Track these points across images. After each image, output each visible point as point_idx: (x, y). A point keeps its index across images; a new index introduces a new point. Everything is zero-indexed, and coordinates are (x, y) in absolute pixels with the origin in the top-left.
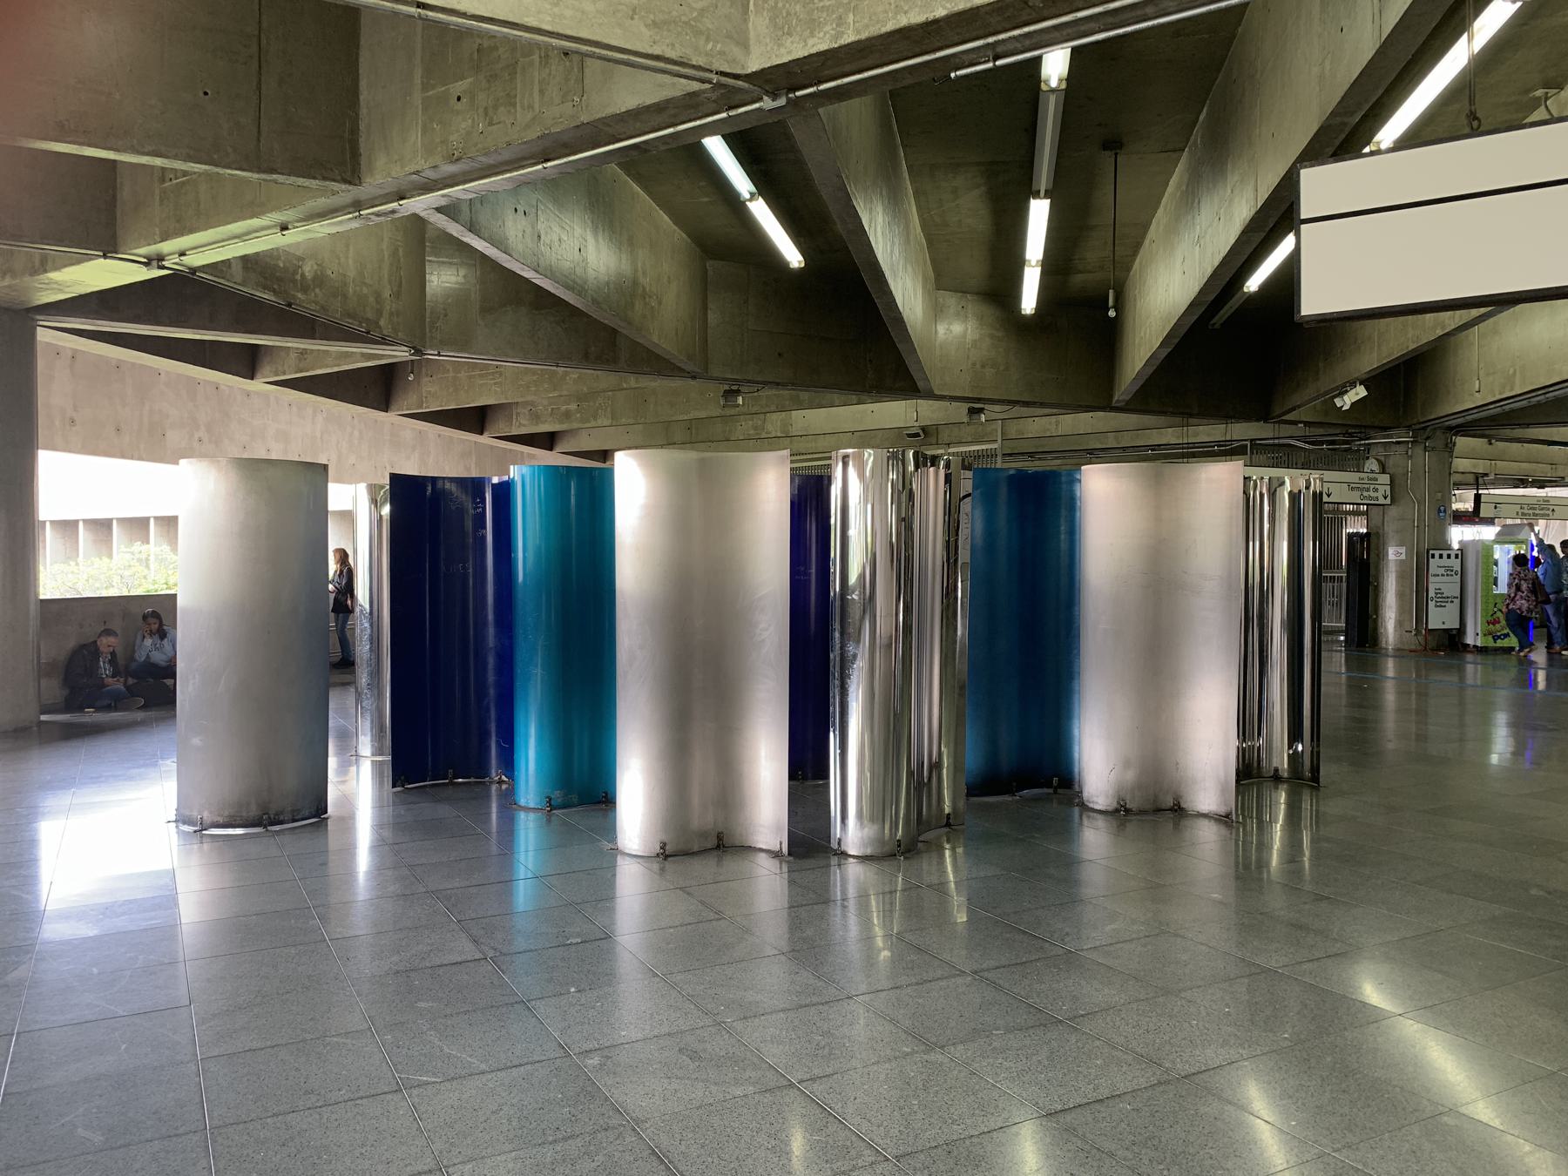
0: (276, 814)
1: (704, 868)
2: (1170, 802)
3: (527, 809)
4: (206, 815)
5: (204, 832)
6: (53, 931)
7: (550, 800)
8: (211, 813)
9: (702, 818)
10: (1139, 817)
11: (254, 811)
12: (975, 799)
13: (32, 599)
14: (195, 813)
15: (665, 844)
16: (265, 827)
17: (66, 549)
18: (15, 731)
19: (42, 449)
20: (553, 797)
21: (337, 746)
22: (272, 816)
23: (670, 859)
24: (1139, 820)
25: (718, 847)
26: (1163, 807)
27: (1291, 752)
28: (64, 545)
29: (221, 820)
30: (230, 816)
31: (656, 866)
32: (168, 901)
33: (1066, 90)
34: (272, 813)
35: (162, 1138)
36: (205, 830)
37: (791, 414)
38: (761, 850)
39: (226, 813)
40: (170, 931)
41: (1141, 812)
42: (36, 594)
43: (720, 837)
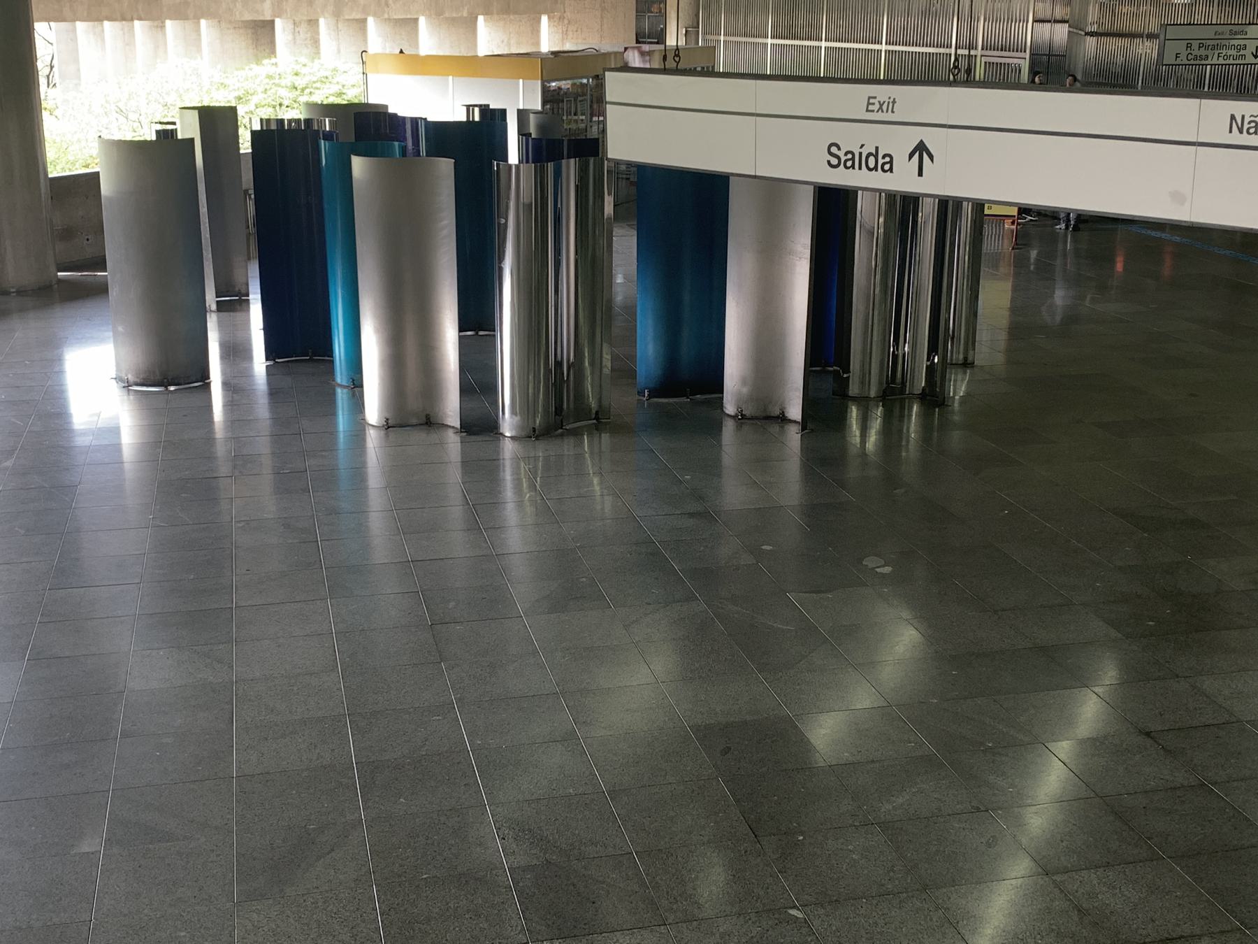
0: (172, 379)
1: (419, 436)
2: (777, 412)
3: (341, 386)
4: (130, 377)
5: (130, 388)
6: (81, 441)
7: (353, 380)
8: (132, 375)
9: (414, 404)
10: (752, 422)
11: (158, 377)
12: (656, 400)
13: (42, 176)
14: (123, 375)
15: (387, 419)
16: (166, 387)
17: (124, 34)
18: (39, 289)
19: (37, 21)
20: (355, 378)
21: (62, 385)
22: (170, 381)
23: (391, 429)
24: (753, 424)
25: (427, 423)
26: (772, 415)
27: (929, 363)
28: (122, 29)
29: (138, 381)
30: (144, 379)
31: (383, 432)
32: (116, 431)
33: (252, 153)
34: (170, 378)
35: (46, 534)
36: (131, 386)
37: (536, 79)
38: (450, 427)
39: (141, 377)
40: (117, 447)
41: (752, 418)
42: (46, 173)
43: (428, 417)
